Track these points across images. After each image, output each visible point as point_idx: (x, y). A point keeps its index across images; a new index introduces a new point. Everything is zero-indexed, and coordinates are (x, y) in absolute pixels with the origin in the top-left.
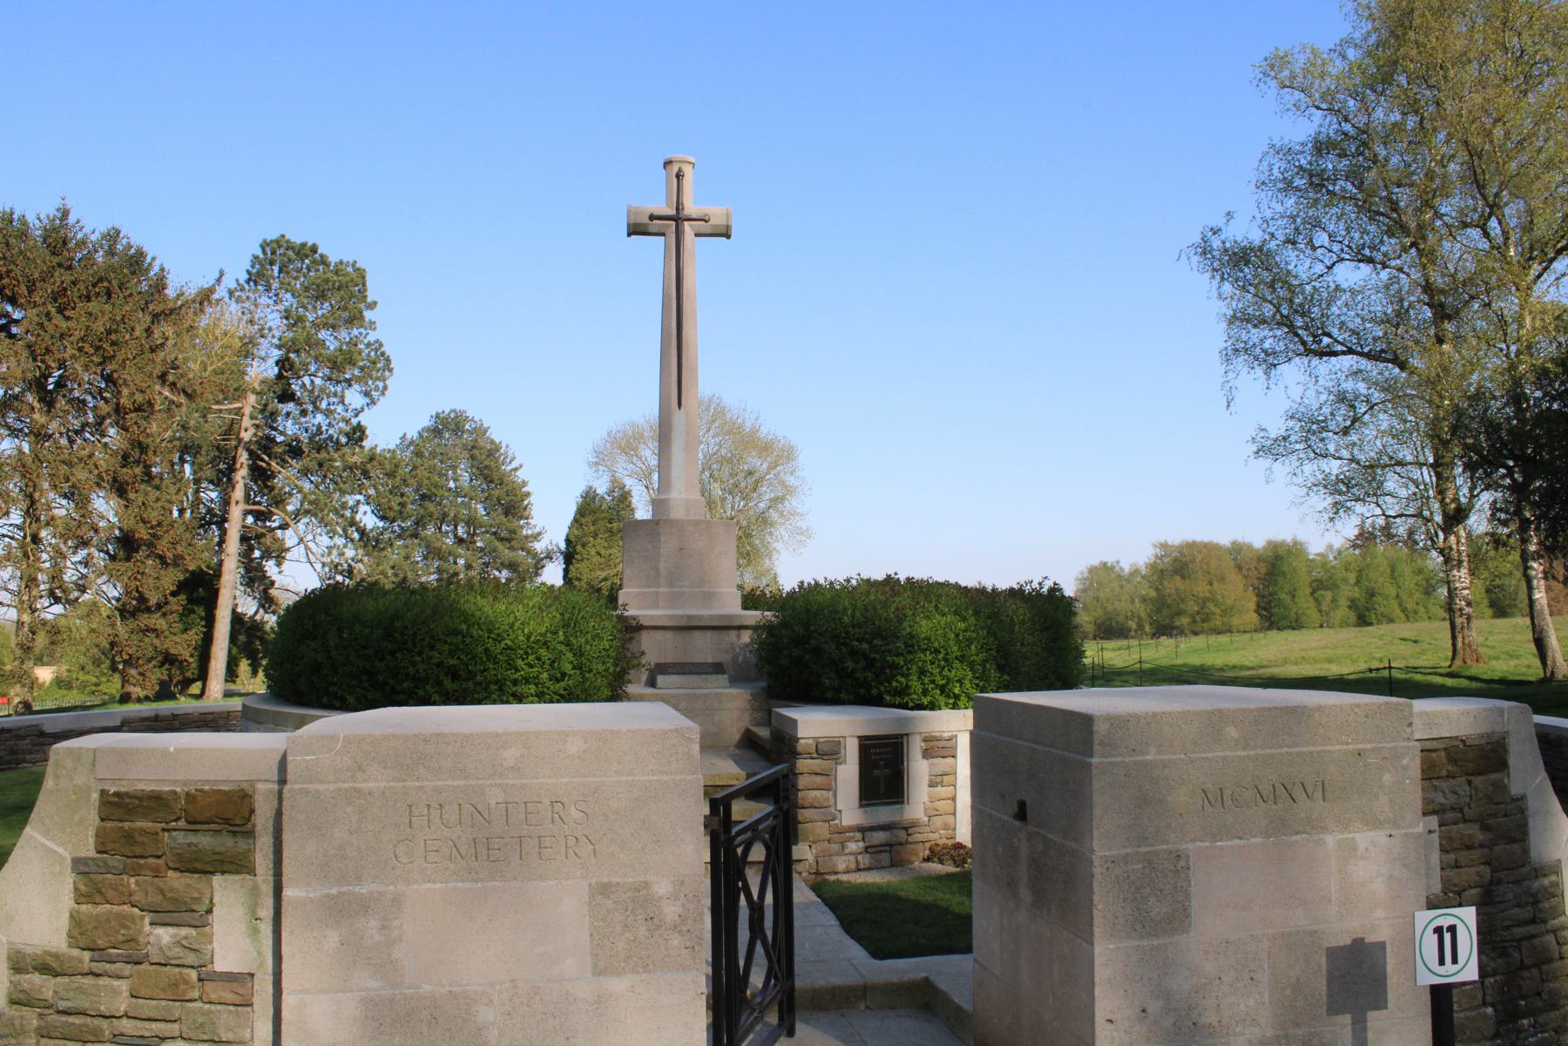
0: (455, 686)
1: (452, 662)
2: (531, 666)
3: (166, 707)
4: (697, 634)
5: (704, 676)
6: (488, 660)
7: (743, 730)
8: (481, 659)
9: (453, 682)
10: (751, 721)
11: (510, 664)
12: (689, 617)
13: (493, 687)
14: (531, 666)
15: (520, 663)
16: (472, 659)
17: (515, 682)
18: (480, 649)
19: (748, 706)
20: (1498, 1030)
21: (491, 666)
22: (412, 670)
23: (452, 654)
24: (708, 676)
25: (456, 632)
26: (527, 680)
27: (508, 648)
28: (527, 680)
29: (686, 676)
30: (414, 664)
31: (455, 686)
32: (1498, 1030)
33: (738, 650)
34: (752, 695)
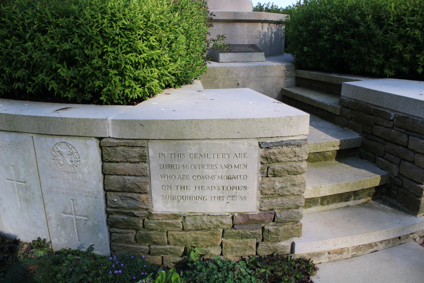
0: (71, 73)
1: (66, 46)
2: (152, 48)
3: (408, 116)
4: (238, 26)
5: (249, 54)
6: (106, 43)
7: (280, 90)
8: (97, 42)
9: (69, 68)
10: (292, 80)
11: (130, 46)
12: (235, 13)
13: (112, 72)
14: (152, 48)
15: (141, 45)
16: (87, 42)
17: (136, 65)
18: (96, 31)
19: (283, 75)
20: (258, 255)
21: (109, 49)
22: (24, 57)
23: (65, 38)
24: (252, 54)
25: (67, 14)
26: (148, 62)
27: (124, 28)
28: (148, 62)
29: (238, 54)
30: (25, 51)
31: (71, 73)
32: (258, 255)
33: (262, 36)
34: (286, 67)
